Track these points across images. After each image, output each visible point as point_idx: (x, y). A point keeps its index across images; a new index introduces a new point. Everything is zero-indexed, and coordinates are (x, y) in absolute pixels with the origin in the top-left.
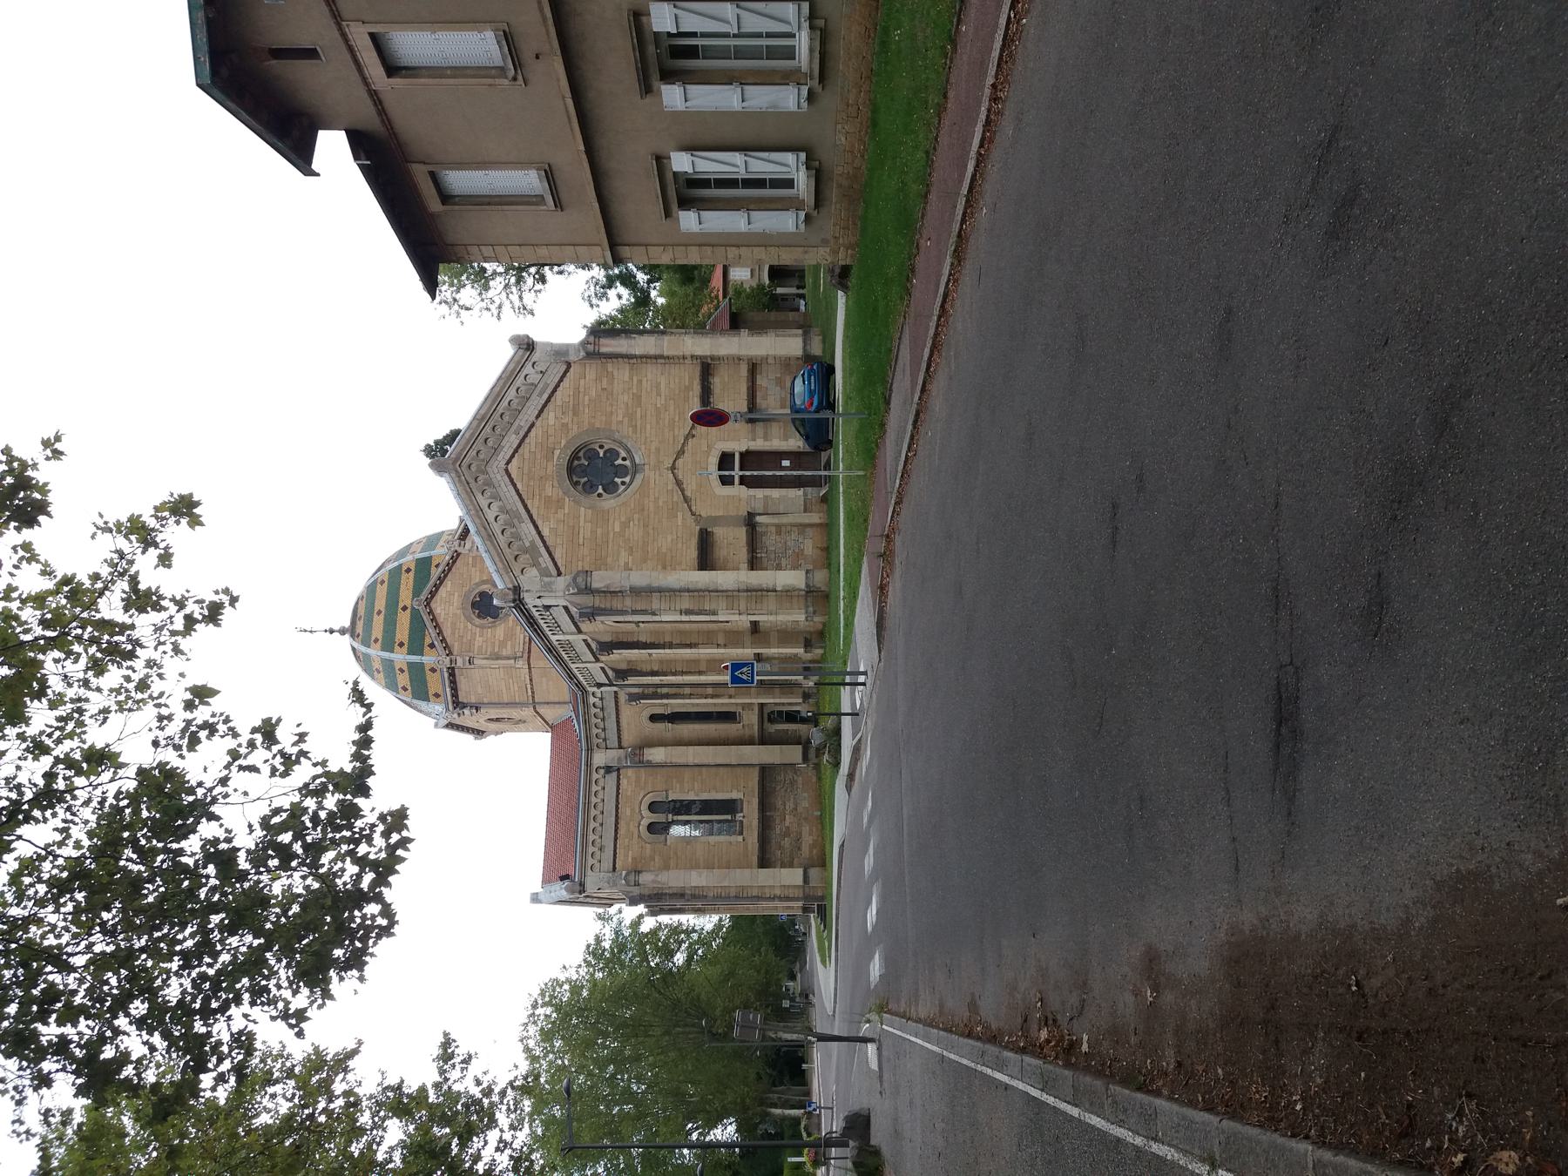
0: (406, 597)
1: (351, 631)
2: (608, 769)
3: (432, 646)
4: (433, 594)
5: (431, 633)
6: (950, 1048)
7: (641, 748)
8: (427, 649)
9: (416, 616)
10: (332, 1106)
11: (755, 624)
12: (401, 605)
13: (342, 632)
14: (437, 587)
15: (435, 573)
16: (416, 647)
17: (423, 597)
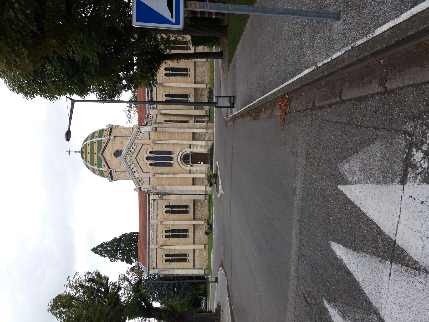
0: (95, 151)
1: (82, 152)
2: (154, 200)
3: (104, 166)
4: (103, 151)
5: (104, 163)
6: (219, 9)
7: (163, 221)
8: (103, 166)
9: (99, 157)
10: (94, 60)
11: (190, 170)
12: (94, 164)
13: (79, 152)
14: (104, 149)
15: (103, 146)
16: (100, 165)
17: (101, 153)
